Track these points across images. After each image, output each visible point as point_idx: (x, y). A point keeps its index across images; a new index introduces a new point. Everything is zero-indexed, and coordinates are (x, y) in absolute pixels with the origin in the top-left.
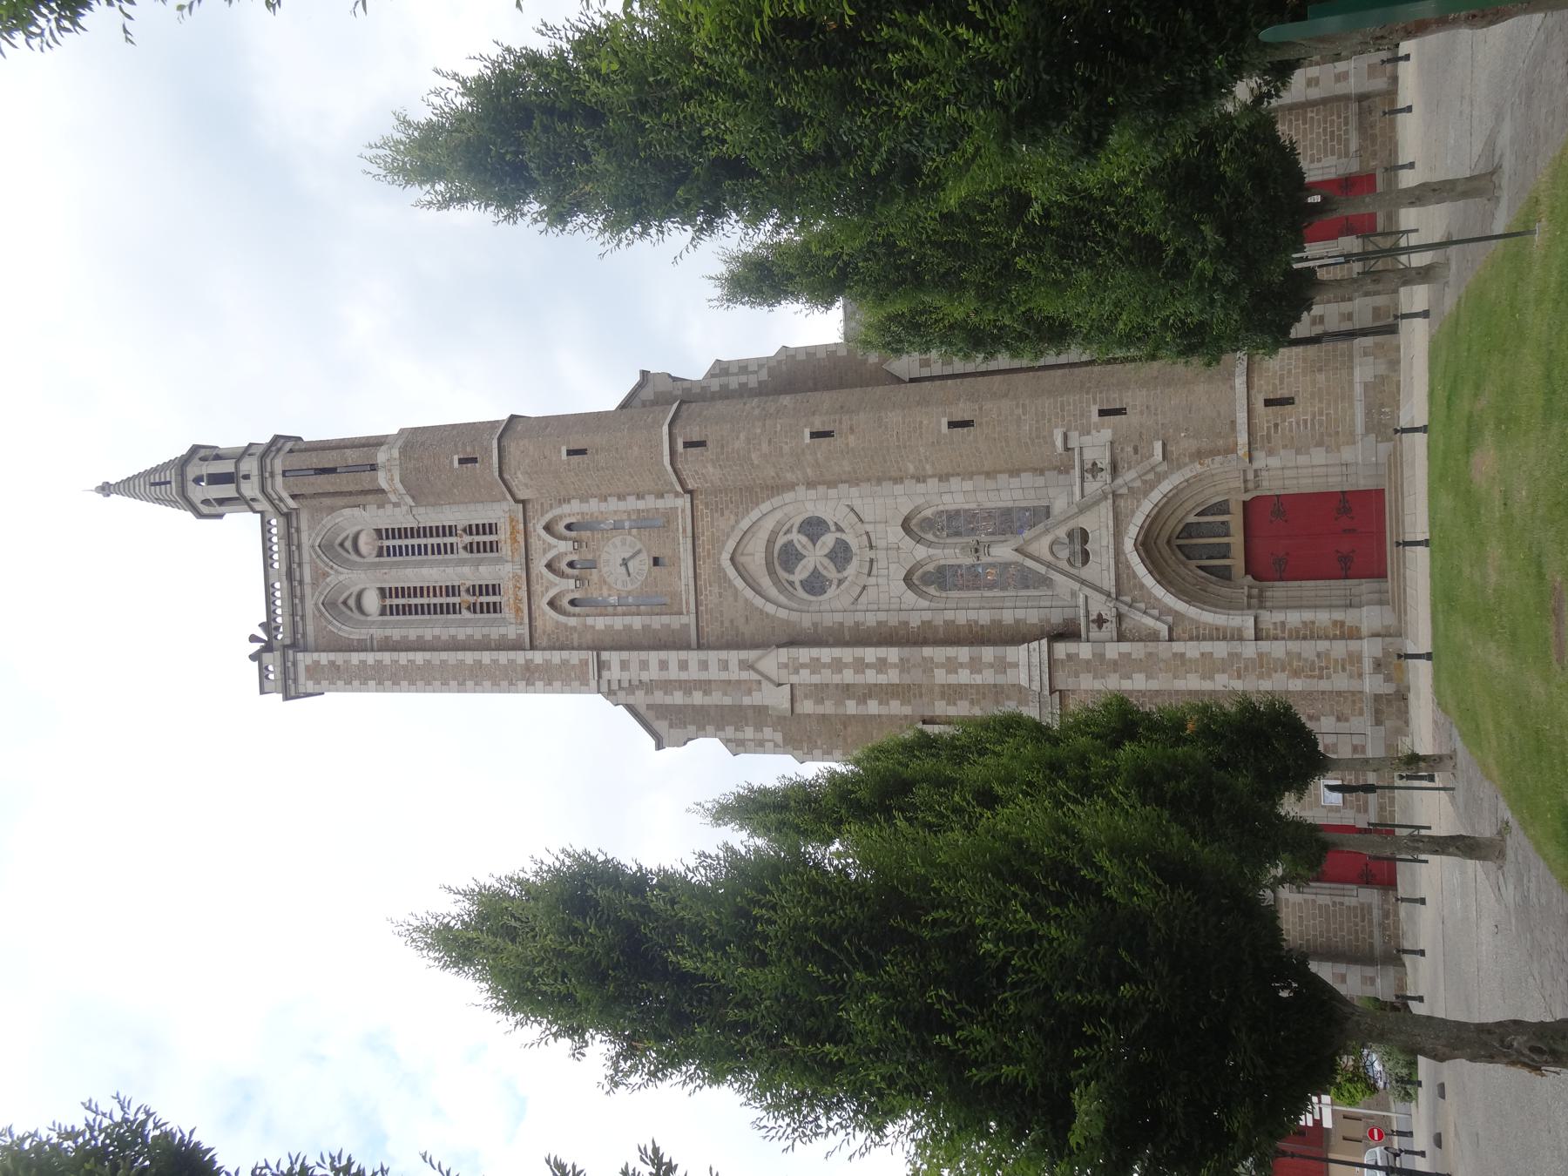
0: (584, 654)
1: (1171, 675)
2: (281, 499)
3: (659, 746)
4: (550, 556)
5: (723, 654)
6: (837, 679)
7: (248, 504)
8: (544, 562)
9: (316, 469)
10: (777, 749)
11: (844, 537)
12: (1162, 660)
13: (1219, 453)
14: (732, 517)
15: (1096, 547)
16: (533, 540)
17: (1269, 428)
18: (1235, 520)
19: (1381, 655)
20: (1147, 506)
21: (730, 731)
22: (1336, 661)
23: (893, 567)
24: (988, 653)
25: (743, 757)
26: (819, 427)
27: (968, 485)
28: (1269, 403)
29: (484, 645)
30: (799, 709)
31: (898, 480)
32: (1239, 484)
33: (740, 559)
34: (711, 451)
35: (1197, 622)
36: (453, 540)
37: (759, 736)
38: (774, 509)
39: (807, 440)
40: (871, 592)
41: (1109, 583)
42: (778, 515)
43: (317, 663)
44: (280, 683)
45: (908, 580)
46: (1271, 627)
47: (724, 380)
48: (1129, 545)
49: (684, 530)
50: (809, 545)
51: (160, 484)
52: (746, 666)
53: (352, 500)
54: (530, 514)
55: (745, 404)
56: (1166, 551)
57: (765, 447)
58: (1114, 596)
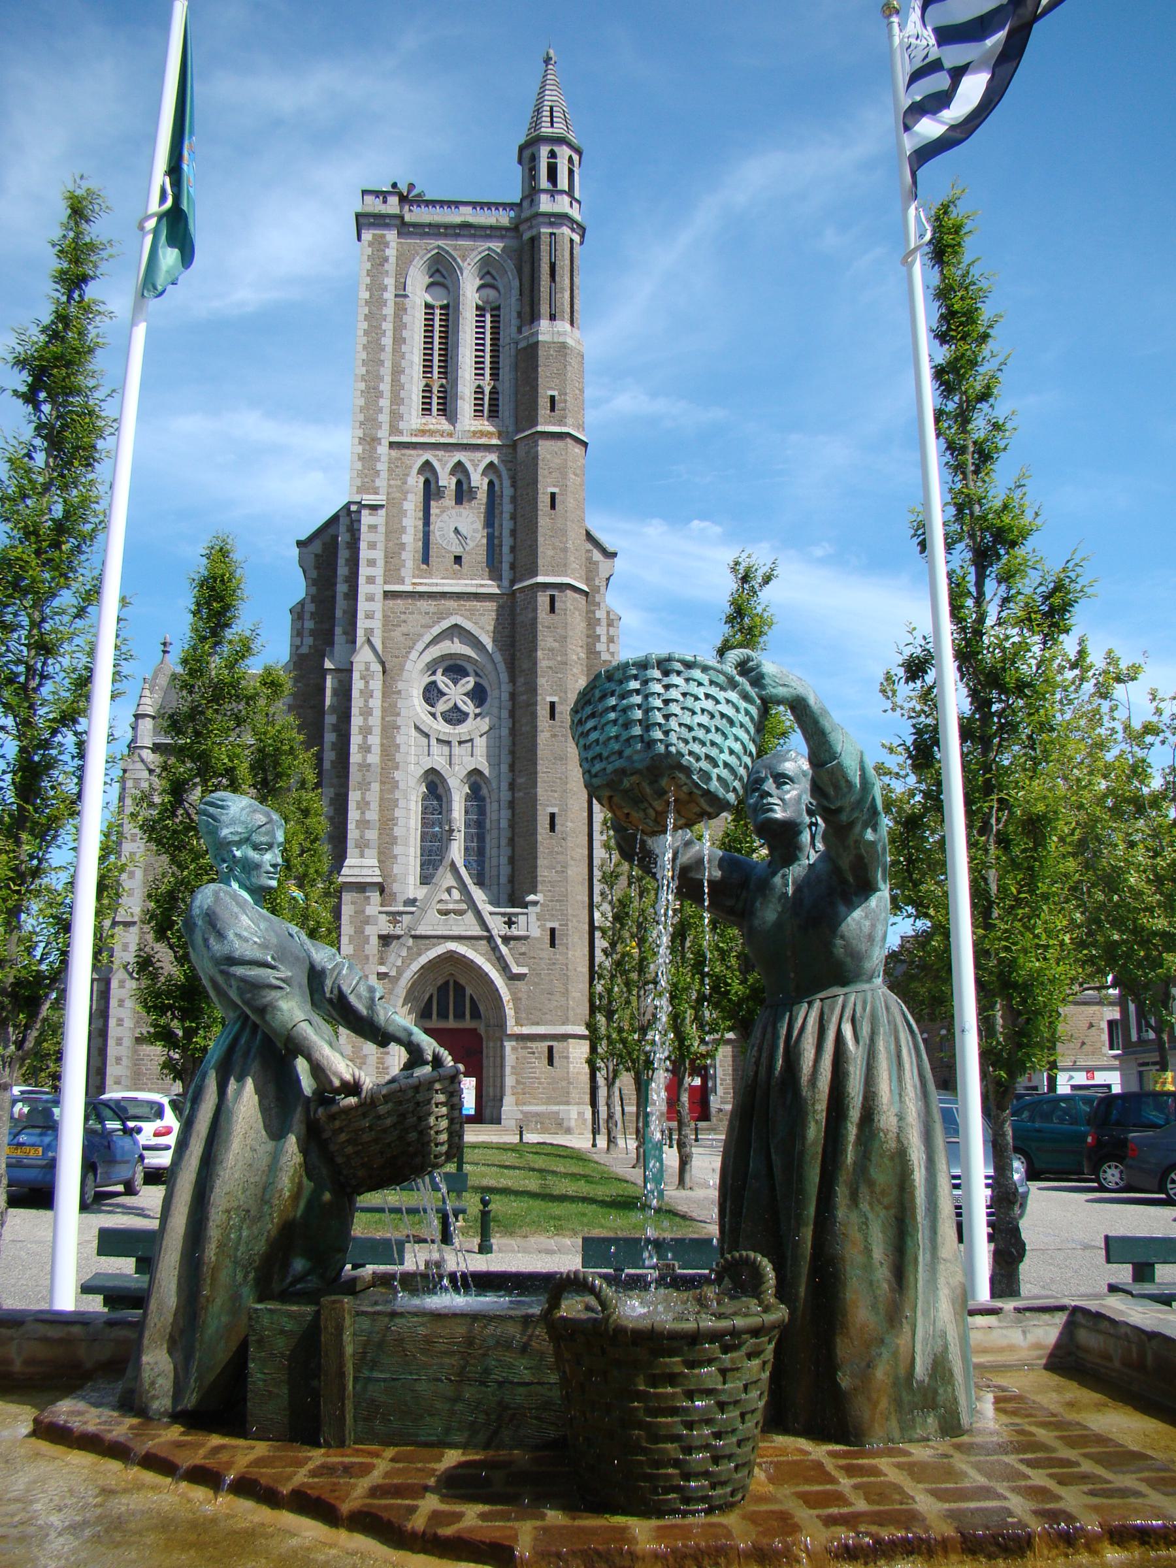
3: (300, 544)
8: (463, 460)
15: (451, 922)
21: (310, 607)
24: (372, 835)
25: (288, 618)
26: (558, 709)
27: (504, 824)
28: (550, 1049)
31: (512, 767)
37: (306, 633)
39: (549, 699)
47: (604, 622)
53: (527, 292)
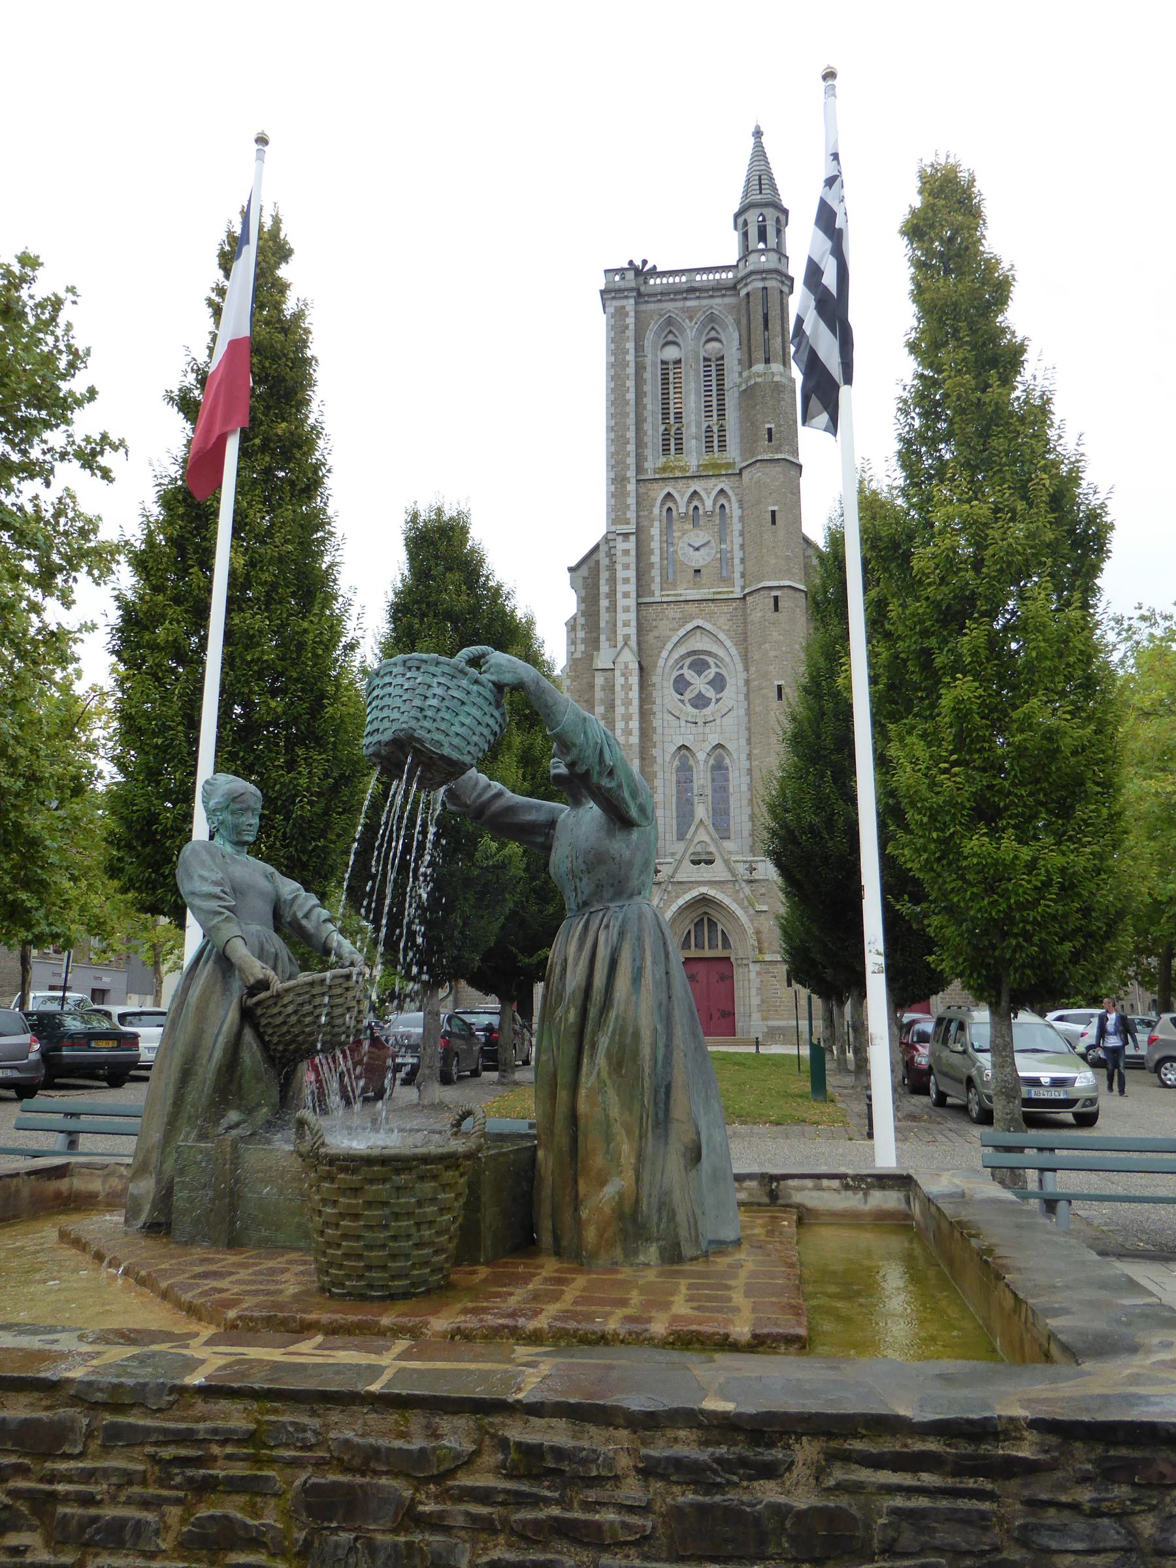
0: (633, 521)
2: (746, 285)
3: (571, 570)
4: (702, 493)
5: (634, 623)
6: (618, 702)
7: (744, 257)
10: (571, 654)
11: (712, 704)
13: (759, 943)
14: (726, 628)
16: (713, 481)
18: (719, 953)
20: (727, 901)
21: (581, 620)
23: (691, 737)
25: (564, 629)
27: (744, 788)
29: (640, 444)
30: (597, 674)
32: (741, 955)
33: (698, 632)
34: (770, 615)
36: (715, 418)
37: (579, 641)
40: (675, 723)
41: (679, 877)
43: (627, 315)
44: (611, 286)
45: (684, 747)
49: (719, 593)
50: (707, 680)
51: (760, 184)
52: (627, 638)
53: (745, 342)
54: (732, 478)
56: (700, 911)
57: (772, 653)
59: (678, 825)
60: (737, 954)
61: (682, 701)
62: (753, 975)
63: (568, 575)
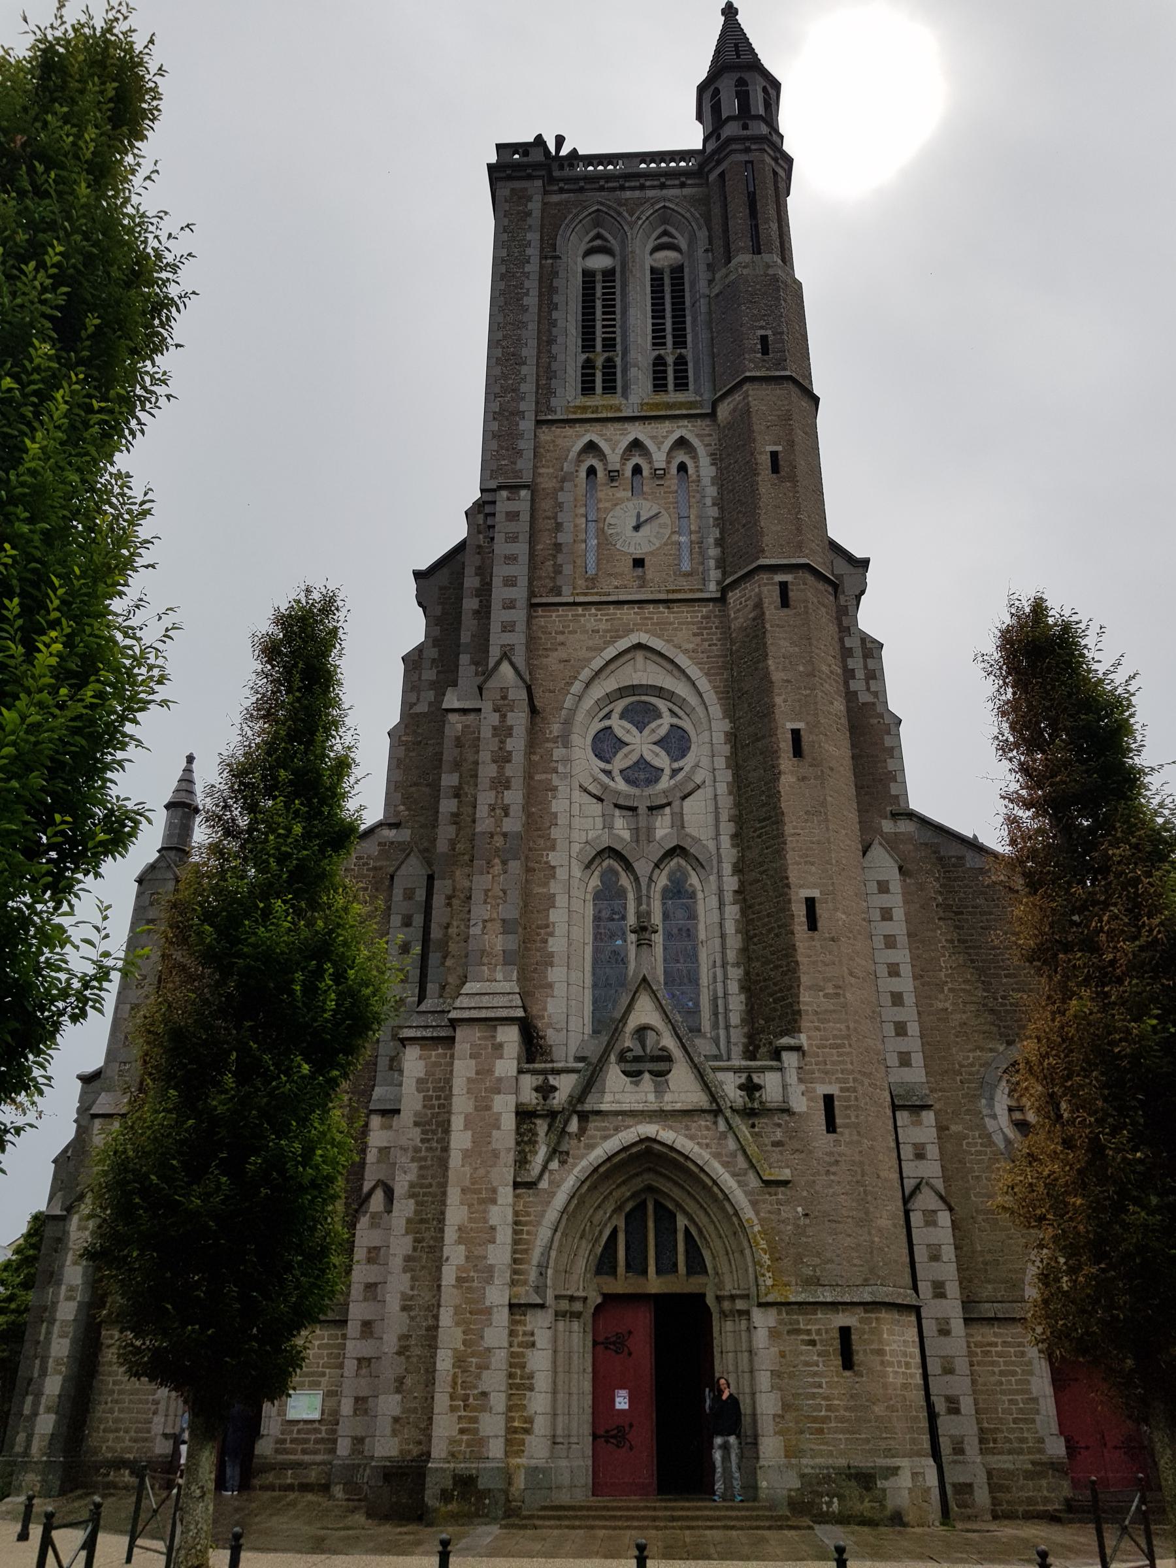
1: (467, 1183)
3: (418, 575)
8: (641, 437)
9: (754, 193)
12: (488, 1172)
14: (691, 646)
17: (808, 1332)
18: (679, 1283)
19: (481, 1487)
21: (433, 653)
22: (475, 1420)
28: (845, 1332)
32: (729, 1288)
33: (640, 655)
35: (539, 1223)
38: (701, 695)
39: (790, 726)
42: (693, 700)
46: (528, 1328)
47: (858, 652)
48: (649, 1129)
50: (656, 737)
55: (834, 657)
56: (638, 1183)
58: (579, 1108)
59: (595, 1002)
60: (720, 1285)
61: (608, 773)
62: (761, 1338)
63: (413, 586)
